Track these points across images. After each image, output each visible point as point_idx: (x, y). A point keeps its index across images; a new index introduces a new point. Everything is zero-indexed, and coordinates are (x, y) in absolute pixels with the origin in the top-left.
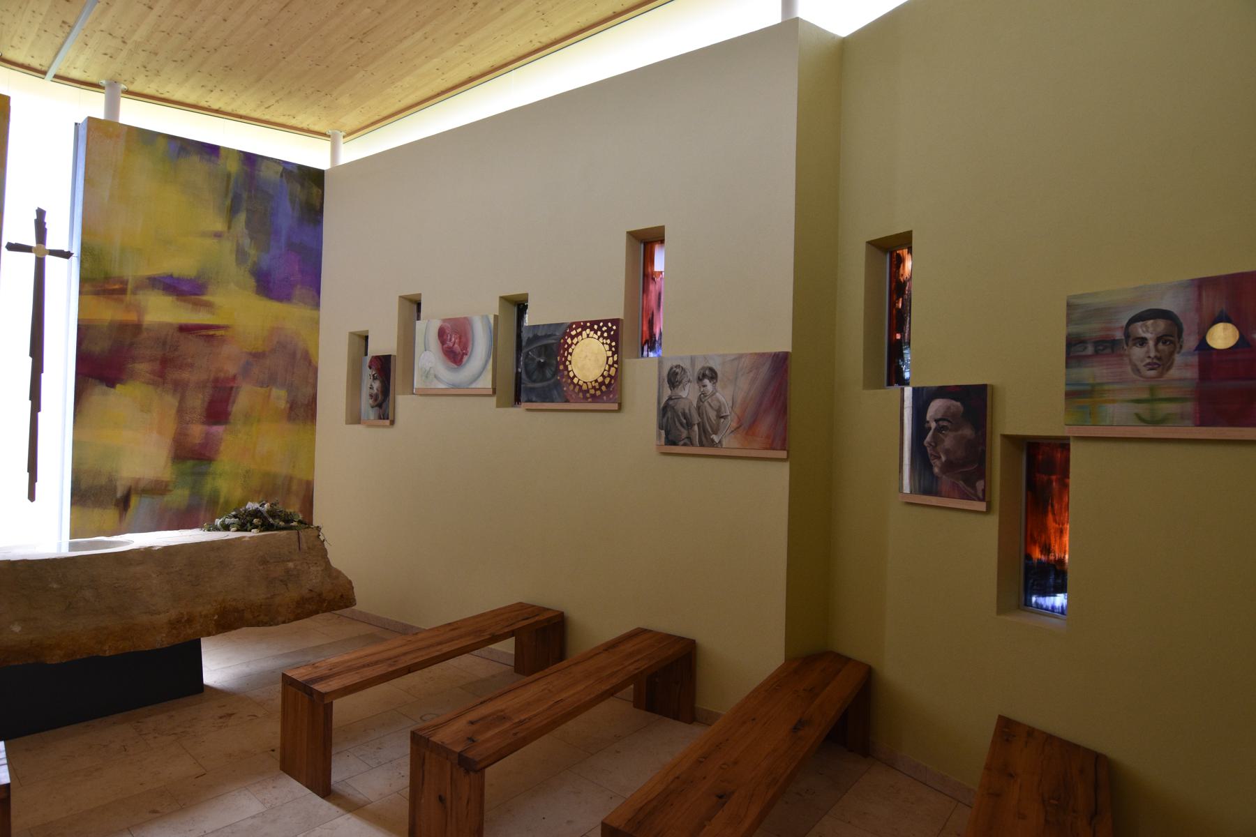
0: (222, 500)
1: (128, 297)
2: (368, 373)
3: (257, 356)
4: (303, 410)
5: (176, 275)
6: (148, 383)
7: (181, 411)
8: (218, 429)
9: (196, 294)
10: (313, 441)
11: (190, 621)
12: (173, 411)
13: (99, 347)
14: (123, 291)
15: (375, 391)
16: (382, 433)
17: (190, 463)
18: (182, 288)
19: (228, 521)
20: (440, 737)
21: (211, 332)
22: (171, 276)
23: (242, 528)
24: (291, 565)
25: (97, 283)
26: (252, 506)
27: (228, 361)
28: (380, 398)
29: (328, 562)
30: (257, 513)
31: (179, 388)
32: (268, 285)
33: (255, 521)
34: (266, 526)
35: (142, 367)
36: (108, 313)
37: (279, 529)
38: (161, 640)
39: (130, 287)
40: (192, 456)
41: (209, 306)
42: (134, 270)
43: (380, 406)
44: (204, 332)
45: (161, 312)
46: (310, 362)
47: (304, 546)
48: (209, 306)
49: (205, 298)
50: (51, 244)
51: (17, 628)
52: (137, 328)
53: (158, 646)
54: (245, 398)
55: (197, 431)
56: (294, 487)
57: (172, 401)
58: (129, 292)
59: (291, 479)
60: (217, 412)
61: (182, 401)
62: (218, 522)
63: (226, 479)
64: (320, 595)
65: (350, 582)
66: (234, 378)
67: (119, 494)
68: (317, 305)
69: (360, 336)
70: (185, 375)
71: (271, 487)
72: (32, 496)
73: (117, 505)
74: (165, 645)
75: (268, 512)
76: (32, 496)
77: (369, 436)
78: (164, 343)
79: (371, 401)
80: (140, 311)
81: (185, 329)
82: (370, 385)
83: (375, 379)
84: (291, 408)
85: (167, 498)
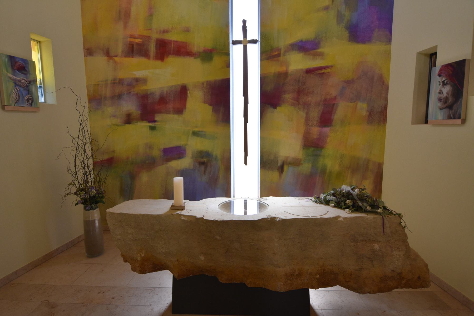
0: (328, 171)
1: (281, 58)
2: (436, 81)
3: (349, 82)
4: (378, 116)
5: (304, 40)
6: (291, 105)
8: (326, 130)
9: (314, 49)
10: (383, 137)
11: (300, 275)
12: (303, 120)
13: (269, 88)
14: (279, 55)
15: (445, 94)
16: (451, 132)
17: (311, 149)
18: (307, 47)
19: (328, 198)
20: (406, 229)
21: (323, 71)
22: (301, 41)
23: (338, 205)
24: (376, 246)
25: (268, 55)
26: (346, 188)
27: (332, 88)
28: (451, 100)
29: (407, 246)
30: (348, 195)
31: (306, 106)
32: (357, 34)
33: (348, 201)
34: (356, 208)
35: (288, 97)
36: (274, 68)
37: (366, 212)
38: (280, 286)
39: (282, 52)
40: (313, 145)
41: (321, 55)
42: (283, 42)
43: (450, 107)
45: (297, 63)
46: (383, 82)
47: (388, 230)
48: (321, 55)
49: (319, 50)
50: (249, 38)
51: (202, 258)
52: (286, 74)
53: (278, 290)
54: (342, 110)
55: (315, 131)
56: (371, 166)
57: (302, 114)
58: (282, 54)
59: (368, 161)
60: (326, 120)
61: (307, 114)
62: (322, 196)
63: (330, 160)
64: (400, 274)
65: (426, 266)
66: (335, 98)
67: (279, 164)
68: (389, 41)
69: (426, 55)
70: (309, 99)
71: (357, 167)
72: (246, 163)
73: (278, 170)
74: (283, 290)
75: (358, 195)
76: (246, 163)
77: (441, 134)
78: (299, 81)
79: (440, 104)
80: (287, 64)
81: (309, 71)
82: (440, 89)
83: (444, 84)
84: (370, 115)
85: (300, 168)
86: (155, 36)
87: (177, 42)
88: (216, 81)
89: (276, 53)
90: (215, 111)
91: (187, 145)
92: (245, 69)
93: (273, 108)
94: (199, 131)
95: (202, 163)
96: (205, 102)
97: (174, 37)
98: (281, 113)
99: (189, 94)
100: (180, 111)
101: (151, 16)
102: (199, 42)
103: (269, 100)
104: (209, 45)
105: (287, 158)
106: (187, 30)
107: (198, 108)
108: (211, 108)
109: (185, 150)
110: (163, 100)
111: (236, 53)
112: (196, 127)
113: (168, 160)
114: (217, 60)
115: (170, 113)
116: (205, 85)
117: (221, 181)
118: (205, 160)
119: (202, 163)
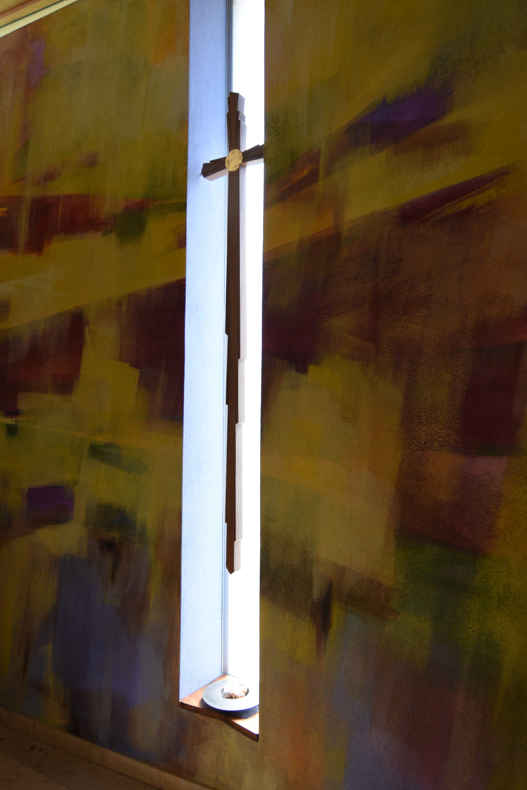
1: (320, 187)
7: (410, 418)
8: (490, 467)
21: (465, 203)
25: (292, 183)
35: (342, 324)
39: (322, 162)
41: (458, 136)
44: (450, 209)
45: (372, 189)
48: (458, 136)
49: (450, 119)
55: (443, 466)
58: (321, 173)
67: (316, 594)
81: (412, 215)
86: (30, 192)
87: (70, 197)
88: (149, 291)
89: (306, 172)
90: (146, 383)
91: (76, 483)
92: (224, 248)
93: (298, 371)
94: (106, 445)
95: (108, 546)
96: (121, 358)
97: (66, 187)
98: (325, 380)
99: (87, 337)
100: (65, 385)
101: (25, 145)
102: (116, 188)
103: (291, 344)
104: (137, 192)
105: (341, 572)
106: (92, 162)
107: (107, 368)
108: (134, 374)
109: (71, 499)
110: (35, 355)
111: (206, 200)
112: (100, 431)
113: (36, 523)
114: (156, 230)
115: (46, 392)
116: (124, 307)
117: (153, 616)
118: (116, 535)
119: (108, 546)
